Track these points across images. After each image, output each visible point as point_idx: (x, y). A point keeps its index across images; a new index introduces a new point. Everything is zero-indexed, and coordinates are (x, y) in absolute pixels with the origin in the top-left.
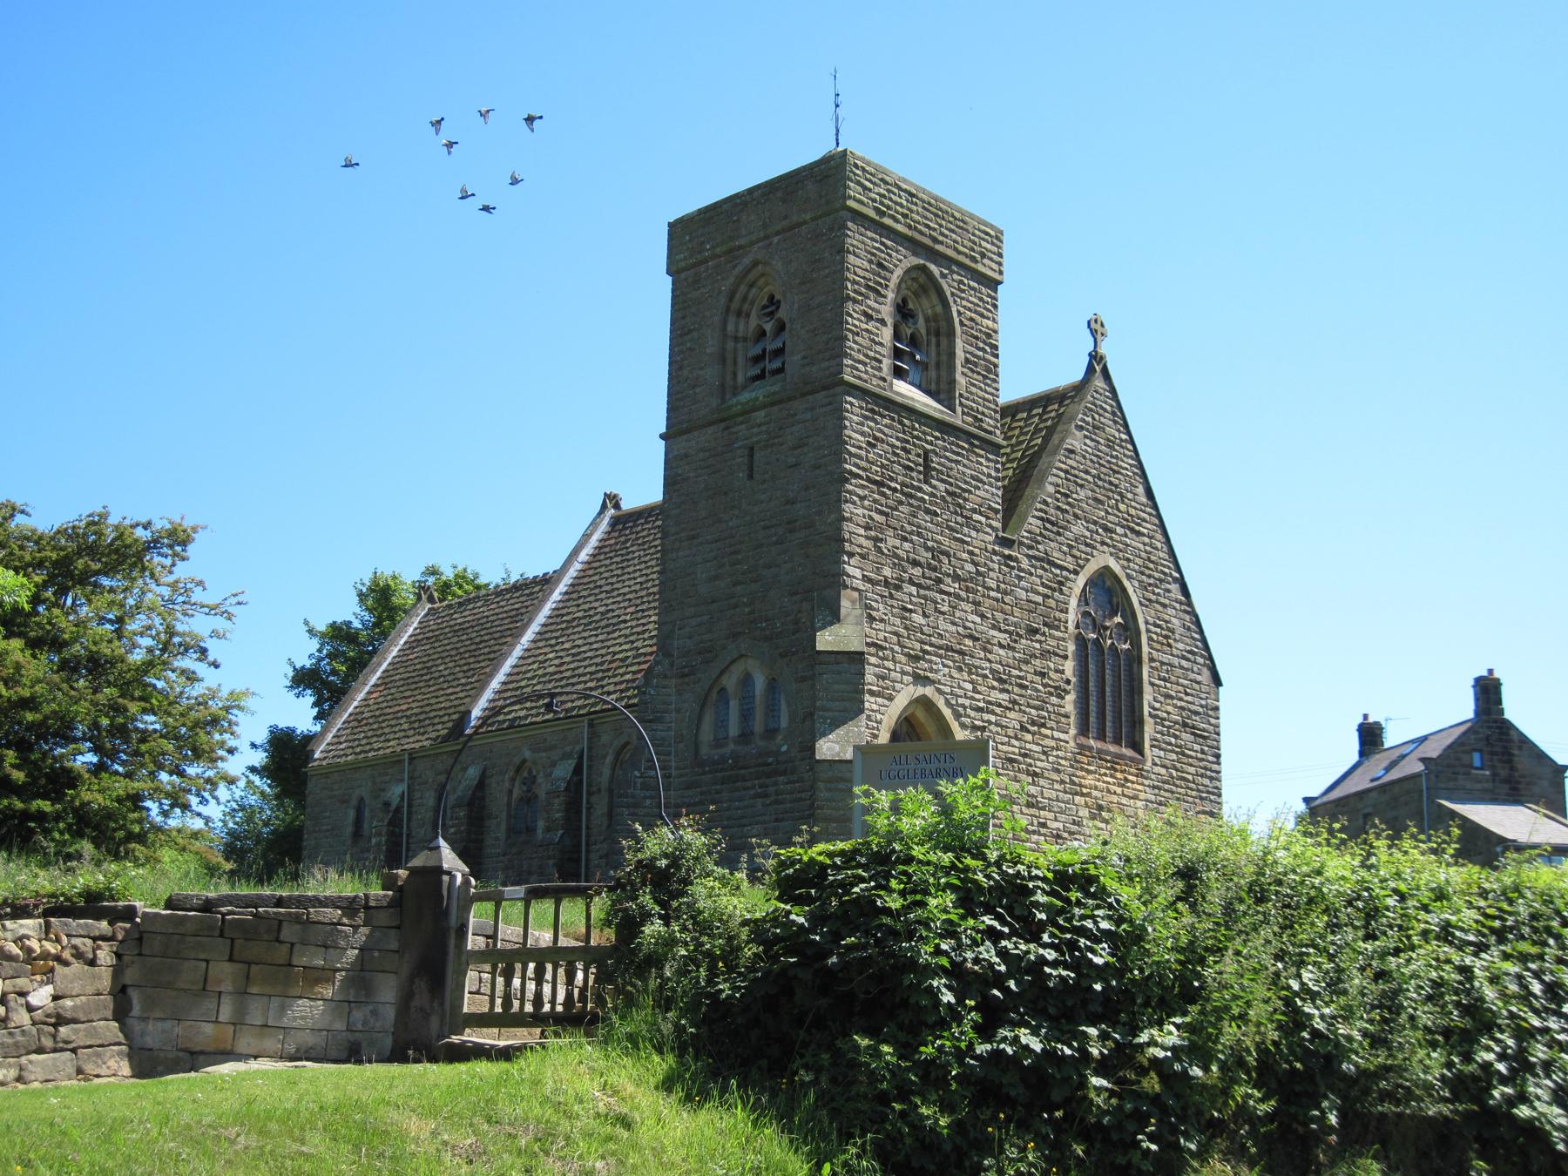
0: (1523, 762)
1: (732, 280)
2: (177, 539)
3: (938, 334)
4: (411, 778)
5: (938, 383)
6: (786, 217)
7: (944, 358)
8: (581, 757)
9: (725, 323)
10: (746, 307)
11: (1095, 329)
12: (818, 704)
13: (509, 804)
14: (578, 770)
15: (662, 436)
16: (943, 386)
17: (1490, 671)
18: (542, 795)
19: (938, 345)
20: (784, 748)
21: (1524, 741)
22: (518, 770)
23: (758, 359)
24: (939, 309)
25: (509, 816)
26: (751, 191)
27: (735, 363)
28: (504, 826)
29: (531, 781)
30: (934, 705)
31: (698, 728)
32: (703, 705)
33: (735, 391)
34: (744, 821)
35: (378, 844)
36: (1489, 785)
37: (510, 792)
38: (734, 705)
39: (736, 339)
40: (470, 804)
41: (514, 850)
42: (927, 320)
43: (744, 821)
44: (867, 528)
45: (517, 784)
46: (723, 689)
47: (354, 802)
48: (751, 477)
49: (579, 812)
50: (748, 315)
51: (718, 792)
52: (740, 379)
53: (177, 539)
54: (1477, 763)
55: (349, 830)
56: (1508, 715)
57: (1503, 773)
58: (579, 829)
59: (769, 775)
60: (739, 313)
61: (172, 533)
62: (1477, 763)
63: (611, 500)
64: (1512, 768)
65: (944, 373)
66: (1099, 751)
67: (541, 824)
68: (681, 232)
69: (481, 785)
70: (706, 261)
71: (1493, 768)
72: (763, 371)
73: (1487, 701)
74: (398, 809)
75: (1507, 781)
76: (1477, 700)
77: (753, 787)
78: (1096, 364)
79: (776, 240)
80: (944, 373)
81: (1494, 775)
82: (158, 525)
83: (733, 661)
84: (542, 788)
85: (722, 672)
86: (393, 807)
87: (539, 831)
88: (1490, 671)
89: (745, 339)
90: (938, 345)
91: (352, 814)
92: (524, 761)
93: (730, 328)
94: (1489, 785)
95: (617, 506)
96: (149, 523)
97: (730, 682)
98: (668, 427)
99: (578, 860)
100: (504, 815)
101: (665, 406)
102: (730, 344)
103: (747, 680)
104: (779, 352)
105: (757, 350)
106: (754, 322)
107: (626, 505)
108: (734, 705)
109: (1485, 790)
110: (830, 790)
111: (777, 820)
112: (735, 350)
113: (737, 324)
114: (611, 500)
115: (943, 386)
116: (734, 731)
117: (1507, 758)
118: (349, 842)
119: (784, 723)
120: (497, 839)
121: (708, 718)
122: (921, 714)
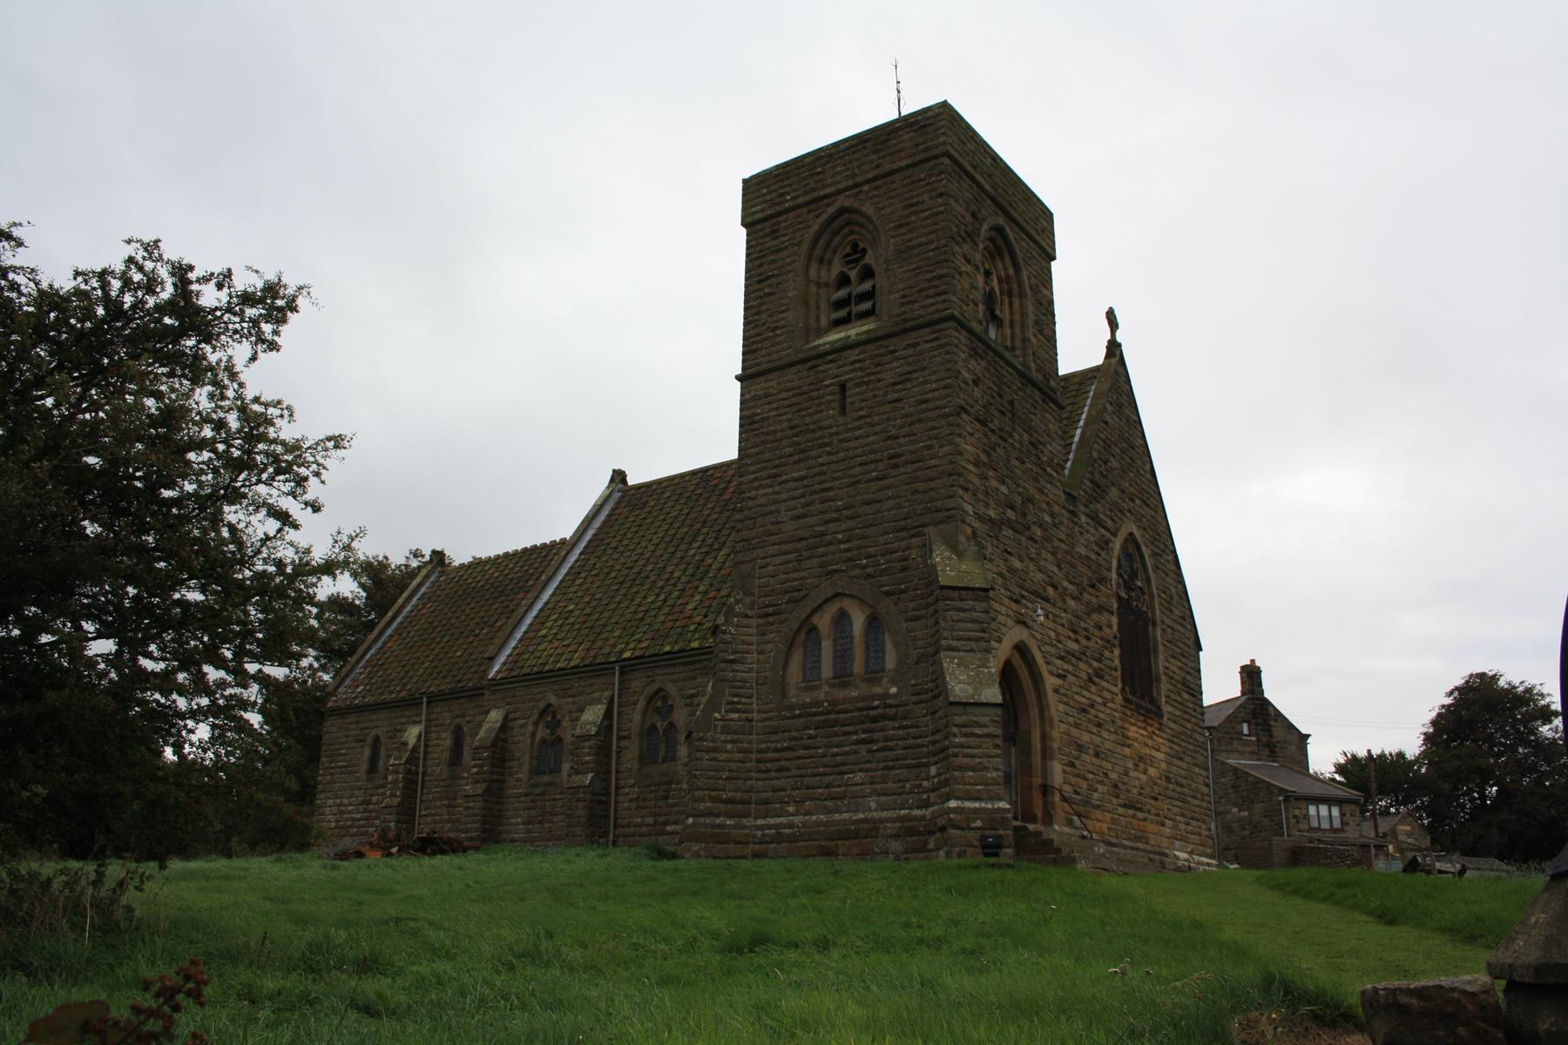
0: (1278, 732)
1: (816, 227)
2: (272, 305)
3: (1010, 295)
4: (428, 720)
5: (1013, 339)
6: (877, 167)
7: (1017, 317)
8: (611, 701)
9: (807, 268)
10: (828, 255)
11: (1111, 317)
12: (944, 642)
13: (532, 746)
14: (608, 714)
15: (738, 378)
16: (1018, 344)
17: (1253, 661)
18: (568, 739)
19: (1011, 304)
20: (894, 690)
21: (1279, 714)
22: (543, 713)
23: (839, 304)
24: (1011, 271)
25: (532, 757)
26: (836, 145)
27: (818, 307)
28: (526, 768)
29: (555, 725)
30: (1029, 651)
31: (785, 670)
32: (791, 646)
33: (820, 333)
34: (844, 768)
35: (395, 782)
36: (1255, 749)
37: (533, 735)
38: (827, 645)
39: (818, 284)
40: (494, 744)
41: (538, 790)
42: (1000, 281)
43: (844, 768)
44: (976, 465)
45: (541, 726)
46: (814, 629)
47: (369, 741)
48: (843, 412)
49: (608, 756)
50: (830, 262)
51: (811, 737)
52: (824, 322)
53: (272, 305)
54: (1246, 731)
55: (364, 766)
56: (1266, 695)
57: (1265, 739)
58: (608, 772)
59: (875, 720)
60: (821, 260)
61: (272, 289)
62: (1246, 731)
63: (619, 476)
64: (1271, 736)
65: (1018, 331)
66: (1137, 705)
67: (566, 766)
68: (755, 188)
69: (504, 727)
70: (786, 211)
71: (1257, 735)
72: (850, 313)
73: (1252, 684)
74: (415, 749)
75: (1268, 745)
76: (1243, 683)
77: (855, 733)
78: (1114, 348)
79: (866, 188)
80: (1018, 331)
81: (1258, 740)
82: (242, 281)
83: (827, 600)
84: (567, 733)
85: (814, 611)
86: (411, 746)
87: (564, 773)
88: (1253, 661)
89: (827, 285)
90: (1011, 304)
91: (367, 752)
92: (550, 705)
93: (813, 273)
94: (1255, 749)
95: (624, 481)
96: (228, 274)
97: (823, 622)
98: (744, 369)
99: (607, 803)
100: (527, 757)
101: (740, 349)
102: (814, 289)
103: (842, 618)
104: (869, 295)
105: (842, 293)
106: (837, 268)
107: (631, 481)
108: (827, 645)
109: (1251, 753)
110: (965, 735)
111: (886, 768)
112: (818, 295)
113: (819, 270)
114: (619, 476)
115: (1018, 344)
116: (827, 670)
117: (1267, 728)
118: (364, 778)
119: (891, 661)
120: (519, 780)
121: (796, 659)
122: (1018, 662)
